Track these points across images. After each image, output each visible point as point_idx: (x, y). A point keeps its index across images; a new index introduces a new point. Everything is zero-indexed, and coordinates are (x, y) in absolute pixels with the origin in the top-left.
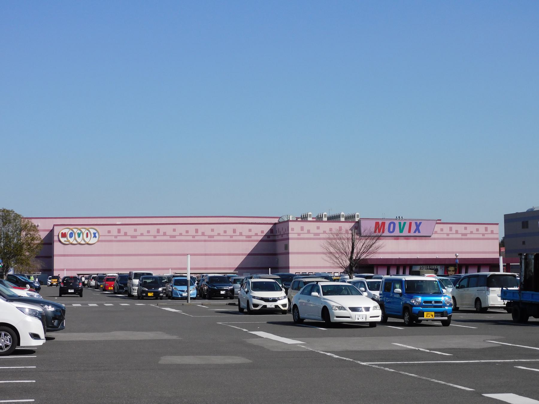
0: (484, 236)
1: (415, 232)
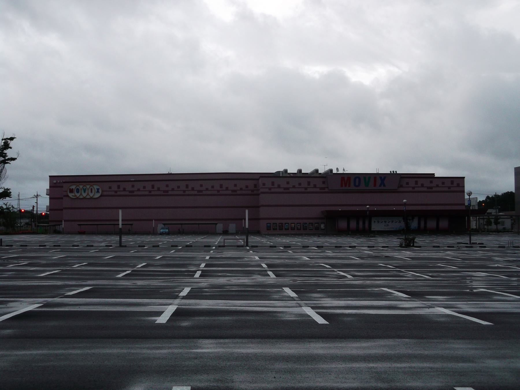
0: (414, 189)
1: (380, 186)
